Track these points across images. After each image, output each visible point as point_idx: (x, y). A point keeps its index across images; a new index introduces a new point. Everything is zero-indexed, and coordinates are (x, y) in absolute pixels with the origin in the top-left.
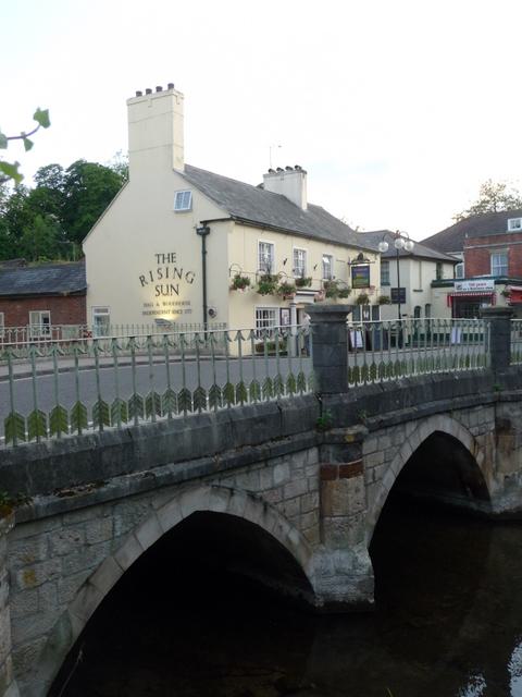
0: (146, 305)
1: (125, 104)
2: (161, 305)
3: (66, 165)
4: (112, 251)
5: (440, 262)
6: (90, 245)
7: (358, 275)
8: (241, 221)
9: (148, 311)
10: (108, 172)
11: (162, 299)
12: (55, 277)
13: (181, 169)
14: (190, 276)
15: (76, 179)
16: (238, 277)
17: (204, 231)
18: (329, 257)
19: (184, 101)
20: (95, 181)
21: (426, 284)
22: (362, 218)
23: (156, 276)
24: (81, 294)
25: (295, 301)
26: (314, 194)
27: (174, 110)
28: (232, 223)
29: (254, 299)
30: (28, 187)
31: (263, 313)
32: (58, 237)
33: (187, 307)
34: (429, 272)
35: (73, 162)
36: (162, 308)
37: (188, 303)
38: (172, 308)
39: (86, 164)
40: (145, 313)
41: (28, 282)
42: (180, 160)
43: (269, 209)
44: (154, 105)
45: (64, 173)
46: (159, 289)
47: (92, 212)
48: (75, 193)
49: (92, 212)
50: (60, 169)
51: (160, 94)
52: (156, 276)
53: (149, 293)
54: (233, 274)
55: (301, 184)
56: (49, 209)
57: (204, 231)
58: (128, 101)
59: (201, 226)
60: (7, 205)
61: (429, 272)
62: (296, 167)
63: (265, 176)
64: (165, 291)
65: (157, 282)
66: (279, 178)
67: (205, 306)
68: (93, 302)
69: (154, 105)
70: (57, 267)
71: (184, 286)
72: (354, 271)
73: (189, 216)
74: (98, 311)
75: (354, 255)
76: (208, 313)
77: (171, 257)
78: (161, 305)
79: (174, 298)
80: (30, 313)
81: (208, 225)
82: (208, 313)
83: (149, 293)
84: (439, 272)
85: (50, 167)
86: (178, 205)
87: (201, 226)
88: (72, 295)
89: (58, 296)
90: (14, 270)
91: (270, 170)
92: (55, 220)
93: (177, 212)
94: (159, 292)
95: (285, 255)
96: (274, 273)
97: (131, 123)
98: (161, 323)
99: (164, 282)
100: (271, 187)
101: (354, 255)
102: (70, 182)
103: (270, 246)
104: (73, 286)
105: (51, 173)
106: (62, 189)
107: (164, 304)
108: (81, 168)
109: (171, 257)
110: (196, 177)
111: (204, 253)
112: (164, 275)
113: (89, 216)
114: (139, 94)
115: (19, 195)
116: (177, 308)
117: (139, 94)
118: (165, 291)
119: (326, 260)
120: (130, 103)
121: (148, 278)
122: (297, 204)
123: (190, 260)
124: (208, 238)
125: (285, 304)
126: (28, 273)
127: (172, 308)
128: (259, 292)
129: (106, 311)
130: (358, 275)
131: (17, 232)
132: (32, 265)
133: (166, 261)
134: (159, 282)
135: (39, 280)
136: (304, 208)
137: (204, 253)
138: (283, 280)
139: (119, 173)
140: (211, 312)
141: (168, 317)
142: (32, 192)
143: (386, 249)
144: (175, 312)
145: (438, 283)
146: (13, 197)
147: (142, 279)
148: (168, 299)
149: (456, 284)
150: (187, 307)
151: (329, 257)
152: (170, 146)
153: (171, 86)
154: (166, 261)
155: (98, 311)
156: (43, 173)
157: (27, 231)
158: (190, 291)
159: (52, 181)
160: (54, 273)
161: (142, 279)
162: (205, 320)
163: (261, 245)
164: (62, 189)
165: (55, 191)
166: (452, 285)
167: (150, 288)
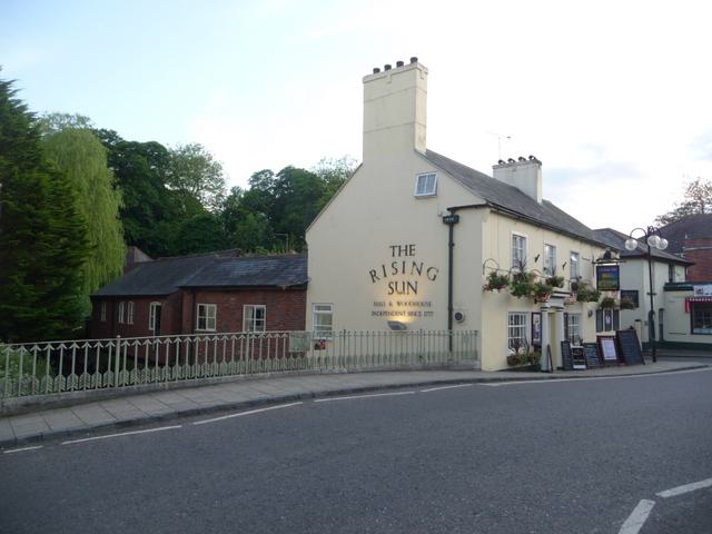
0: (376, 304)
1: (361, 82)
2: (395, 305)
3: (276, 170)
4: (329, 242)
5: (672, 264)
6: (313, 236)
7: (604, 276)
8: (498, 210)
9: (379, 311)
10: (313, 176)
11: (395, 297)
12: (272, 268)
13: (424, 152)
14: (432, 273)
15: (285, 182)
16: (494, 275)
17: (452, 219)
18: (576, 254)
19: (429, 76)
20: (301, 184)
21: (659, 287)
22: (593, 218)
23: (389, 270)
24: (301, 289)
25: (547, 305)
26: (549, 192)
27: (418, 85)
28: (488, 210)
29: (507, 301)
30: (243, 189)
31: (516, 319)
32: (266, 232)
33: (427, 309)
34: (661, 273)
35: (286, 166)
36: (395, 308)
37: (429, 304)
38: (408, 309)
39: (294, 170)
40: (374, 313)
41: (244, 273)
42: (423, 140)
43: (511, 198)
44: (394, 88)
45: (274, 178)
46: (394, 287)
47: (296, 211)
48: (283, 194)
49: (296, 211)
50: (271, 174)
51: (401, 69)
52: (389, 270)
53: (381, 291)
54: (488, 272)
55: (536, 177)
56: (260, 209)
57: (452, 219)
58: (365, 78)
59: (449, 214)
60: (225, 204)
61: (661, 273)
62: (531, 157)
63: (495, 168)
64: (400, 288)
65: (390, 277)
66: (511, 169)
67: (451, 309)
68: (314, 297)
69: (394, 88)
70: (273, 258)
71: (423, 283)
72: (600, 271)
73: (434, 201)
74: (319, 308)
75: (599, 253)
76: (455, 317)
77: (410, 250)
78: (395, 305)
79: (411, 297)
80: (245, 306)
81: (459, 213)
82: (455, 317)
83: (381, 291)
84: (671, 273)
85: (263, 172)
86: (420, 189)
87: (449, 214)
88: (291, 290)
89: (275, 289)
90: (230, 260)
91: (500, 161)
92: (264, 218)
93: (417, 198)
94: (392, 288)
95: (543, 253)
96: (528, 270)
97: (367, 101)
98: (396, 326)
99: (399, 278)
100: (503, 177)
101: (599, 253)
102: (279, 185)
103: (522, 238)
104: (292, 279)
105: (263, 177)
106: (272, 192)
107: (399, 304)
108: (290, 174)
109: (410, 250)
110: (431, 157)
111: (451, 245)
112: (400, 270)
113: (294, 214)
114: (376, 71)
115: (235, 196)
116: (413, 309)
117: (376, 71)
118: (400, 288)
119: (574, 258)
120: (366, 81)
121: (380, 273)
122: (531, 195)
123: (431, 246)
124: (458, 229)
125: (536, 308)
126: (243, 264)
127: (408, 309)
128: (514, 294)
129: (329, 308)
130: (604, 276)
131: (232, 227)
132: (247, 255)
133: (403, 253)
134: (394, 278)
135: (254, 271)
136: (539, 201)
137: (451, 245)
138: (537, 280)
139: (323, 178)
140: (459, 316)
141: (402, 319)
142: (246, 193)
143: (635, 247)
144: (411, 314)
145: (671, 287)
146: (229, 198)
147: (373, 274)
148: (403, 298)
149: (696, 287)
150: (427, 309)
151: (576, 254)
152: (412, 124)
153: (414, 60)
154: (403, 253)
155: (319, 308)
156: (256, 177)
157: (240, 227)
158: (432, 291)
159: (264, 184)
160: (272, 265)
161: (373, 274)
162: (450, 328)
163: (515, 237)
164: (272, 192)
165: (266, 193)
166: (692, 289)
167: (383, 284)
